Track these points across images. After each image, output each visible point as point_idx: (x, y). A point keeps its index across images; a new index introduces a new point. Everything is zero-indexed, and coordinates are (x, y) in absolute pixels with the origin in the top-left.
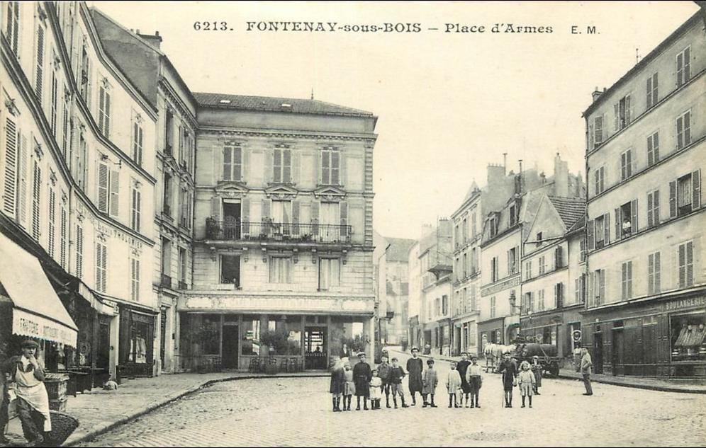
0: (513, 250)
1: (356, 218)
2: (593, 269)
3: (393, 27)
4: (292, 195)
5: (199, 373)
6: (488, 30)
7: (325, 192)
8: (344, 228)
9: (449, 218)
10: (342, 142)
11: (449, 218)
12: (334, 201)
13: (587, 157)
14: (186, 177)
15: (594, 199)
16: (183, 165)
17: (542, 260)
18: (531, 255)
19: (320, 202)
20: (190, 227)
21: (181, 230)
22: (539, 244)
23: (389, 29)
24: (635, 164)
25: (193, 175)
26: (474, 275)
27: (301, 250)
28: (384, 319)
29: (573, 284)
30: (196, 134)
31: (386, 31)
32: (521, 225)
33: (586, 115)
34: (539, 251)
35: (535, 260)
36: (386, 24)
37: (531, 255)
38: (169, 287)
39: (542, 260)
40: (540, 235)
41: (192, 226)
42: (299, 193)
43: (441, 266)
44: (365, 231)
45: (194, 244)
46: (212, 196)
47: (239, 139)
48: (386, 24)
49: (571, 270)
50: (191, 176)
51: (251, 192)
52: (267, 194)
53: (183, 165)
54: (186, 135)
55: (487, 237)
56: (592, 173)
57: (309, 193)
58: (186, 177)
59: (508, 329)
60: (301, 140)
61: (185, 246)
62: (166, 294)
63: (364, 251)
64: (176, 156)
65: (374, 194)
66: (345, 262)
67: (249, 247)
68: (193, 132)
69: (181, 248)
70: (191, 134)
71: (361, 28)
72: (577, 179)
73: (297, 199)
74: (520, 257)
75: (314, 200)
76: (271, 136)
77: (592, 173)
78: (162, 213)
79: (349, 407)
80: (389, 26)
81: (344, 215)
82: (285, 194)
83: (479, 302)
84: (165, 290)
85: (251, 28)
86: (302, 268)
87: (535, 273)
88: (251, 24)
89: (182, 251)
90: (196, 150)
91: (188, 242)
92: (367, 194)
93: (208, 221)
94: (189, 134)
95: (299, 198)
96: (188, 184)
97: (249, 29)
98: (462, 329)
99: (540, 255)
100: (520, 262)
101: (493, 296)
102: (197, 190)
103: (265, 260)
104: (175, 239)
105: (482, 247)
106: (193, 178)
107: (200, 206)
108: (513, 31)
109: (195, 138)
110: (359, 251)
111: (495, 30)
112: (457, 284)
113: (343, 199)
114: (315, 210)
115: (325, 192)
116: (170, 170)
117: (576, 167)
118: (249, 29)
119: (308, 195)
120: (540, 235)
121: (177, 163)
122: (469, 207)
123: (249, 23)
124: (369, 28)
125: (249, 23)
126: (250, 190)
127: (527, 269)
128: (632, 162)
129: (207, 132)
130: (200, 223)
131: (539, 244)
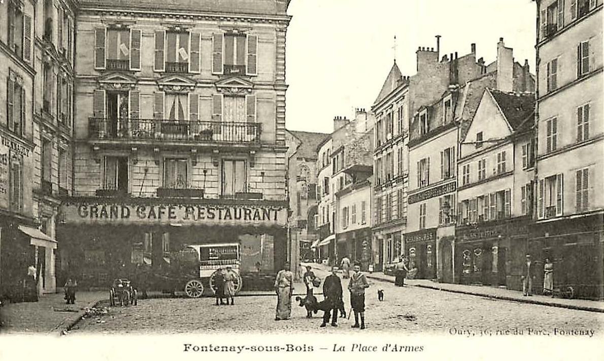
0: (448, 151)
1: (265, 115)
2: (542, 176)
3: (257, 348)
4: (190, 87)
5: (84, 291)
6: (380, 349)
7: (229, 83)
8: (255, 127)
9: (368, 109)
10: (249, 24)
11: (368, 109)
12: (240, 94)
13: (538, 47)
14: (66, 66)
15: (546, 97)
16: (62, 53)
17: (482, 164)
18: (470, 157)
19: (222, 95)
20: (70, 125)
21: (61, 128)
22: (478, 145)
23: (290, 349)
24: (594, 60)
25: (72, 62)
26: (401, 179)
27: (202, 151)
28: (295, 229)
29: (519, 192)
30: (75, 15)
31: (288, 350)
32: (458, 123)
33: (535, 47)
34: (478, 154)
35: (474, 163)
36: (288, 345)
37: (470, 157)
38: (50, 194)
39: (482, 164)
40: (480, 135)
41: (72, 125)
42: (198, 85)
43: (359, 166)
44: (277, 129)
45: (74, 143)
46: (94, 88)
47: (125, 21)
48: (288, 345)
49: (516, 176)
50: (70, 64)
51: (140, 83)
52: (159, 86)
53: (62, 53)
54: (66, 17)
55: (417, 134)
56: (543, 67)
57: (210, 85)
58: (66, 66)
59: (441, 241)
60: (200, 22)
61: (63, 145)
62: (47, 202)
63: (275, 152)
64: (55, 42)
65: (288, 86)
66: (252, 165)
67: (139, 147)
68: (73, 14)
69: (44, 138)
70: (71, 16)
71: (265, 349)
72: (524, 68)
73: (195, 93)
74: (456, 160)
75: (215, 93)
76: (165, 17)
77: (543, 67)
78: (41, 111)
79: (363, 324)
80: (290, 346)
81: (250, 111)
82: (181, 86)
83: (405, 210)
84: (46, 197)
85: (187, 349)
86: (201, 172)
87: (474, 177)
88: (187, 346)
89: (61, 151)
90: (75, 34)
91: (68, 143)
92: (280, 85)
93: (91, 121)
94: (69, 16)
95: (198, 91)
96: (67, 74)
97: (186, 350)
98: (384, 241)
99: (479, 158)
100: (456, 165)
101: (422, 203)
102: (77, 81)
103: (157, 163)
104: (55, 140)
105: (410, 145)
106: (72, 66)
107: (80, 101)
108: (239, 347)
109: (75, 20)
110: (269, 152)
111: (385, 349)
112: (378, 188)
113: (250, 93)
114: (217, 108)
115: (229, 83)
116: (49, 59)
117: (525, 52)
118: (186, 350)
119: (209, 87)
120: (480, 135)
121: (57, 49)
122: (395, 99)
123: (186, 345)
124: (273, 349)
125: (186, 345)
126: (139, 81)
127: (464, 173)
128: (590, 56)
129: (89, 13)
130: (81, 122)
131: (478, 145)
